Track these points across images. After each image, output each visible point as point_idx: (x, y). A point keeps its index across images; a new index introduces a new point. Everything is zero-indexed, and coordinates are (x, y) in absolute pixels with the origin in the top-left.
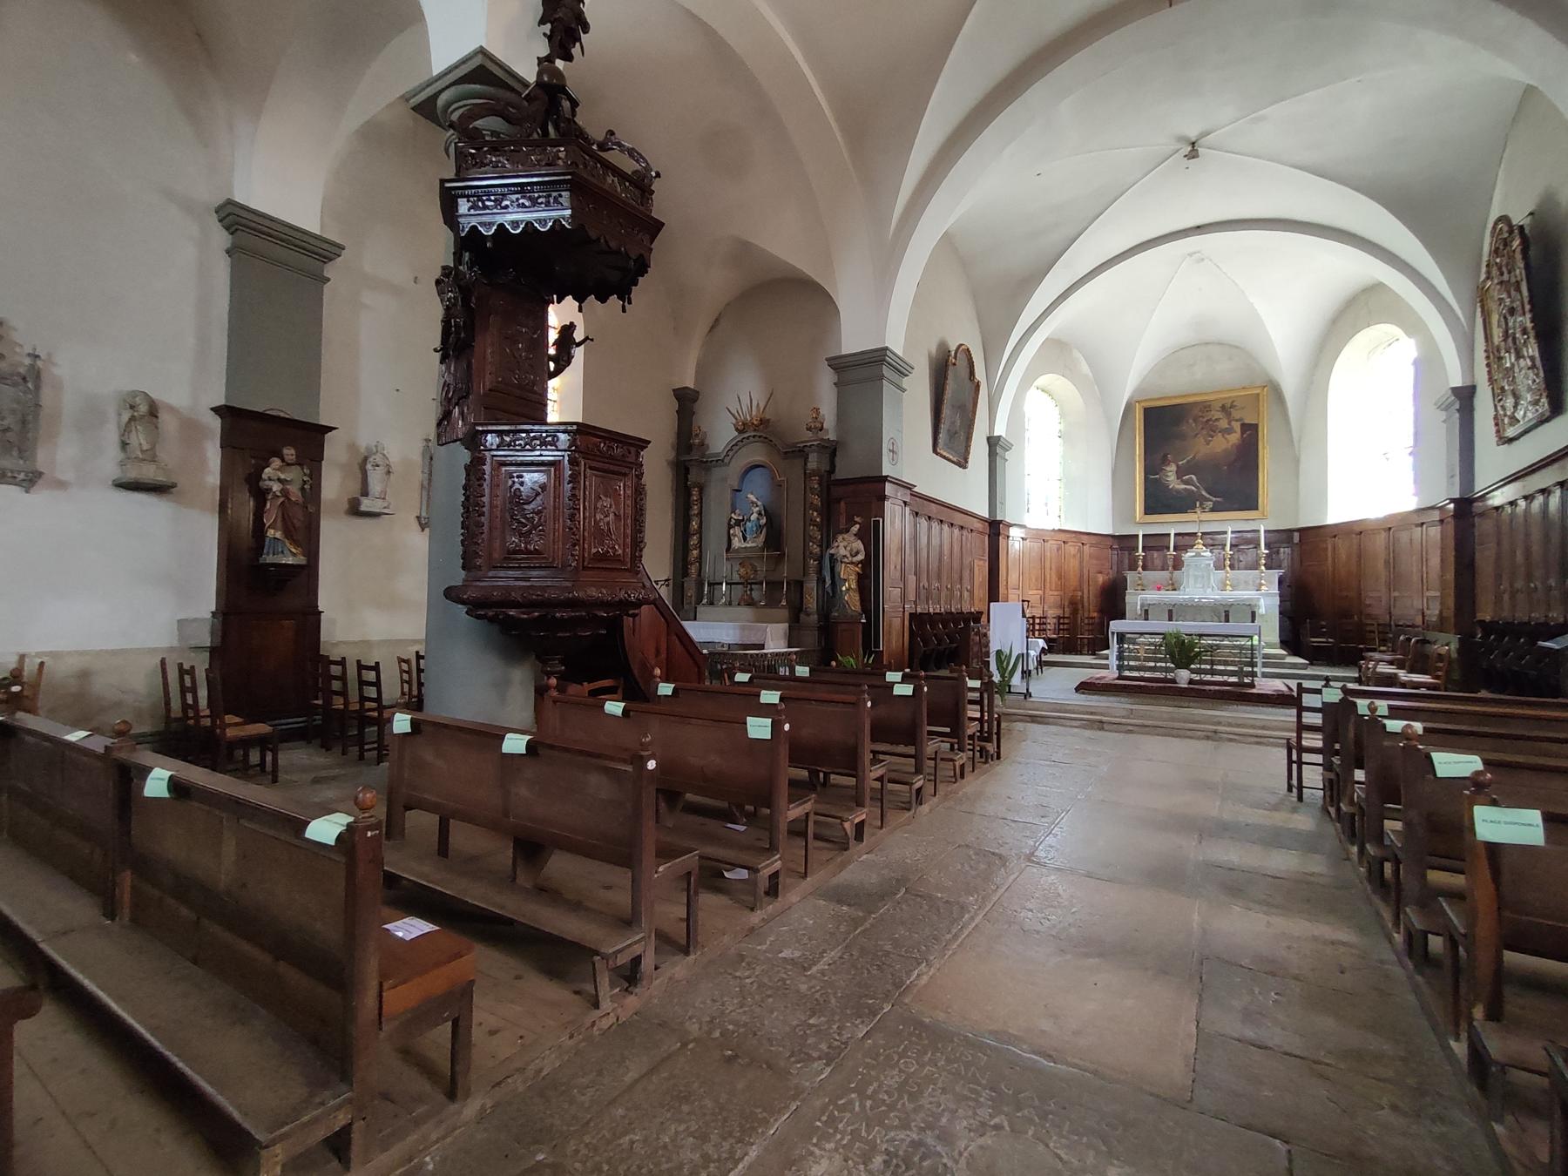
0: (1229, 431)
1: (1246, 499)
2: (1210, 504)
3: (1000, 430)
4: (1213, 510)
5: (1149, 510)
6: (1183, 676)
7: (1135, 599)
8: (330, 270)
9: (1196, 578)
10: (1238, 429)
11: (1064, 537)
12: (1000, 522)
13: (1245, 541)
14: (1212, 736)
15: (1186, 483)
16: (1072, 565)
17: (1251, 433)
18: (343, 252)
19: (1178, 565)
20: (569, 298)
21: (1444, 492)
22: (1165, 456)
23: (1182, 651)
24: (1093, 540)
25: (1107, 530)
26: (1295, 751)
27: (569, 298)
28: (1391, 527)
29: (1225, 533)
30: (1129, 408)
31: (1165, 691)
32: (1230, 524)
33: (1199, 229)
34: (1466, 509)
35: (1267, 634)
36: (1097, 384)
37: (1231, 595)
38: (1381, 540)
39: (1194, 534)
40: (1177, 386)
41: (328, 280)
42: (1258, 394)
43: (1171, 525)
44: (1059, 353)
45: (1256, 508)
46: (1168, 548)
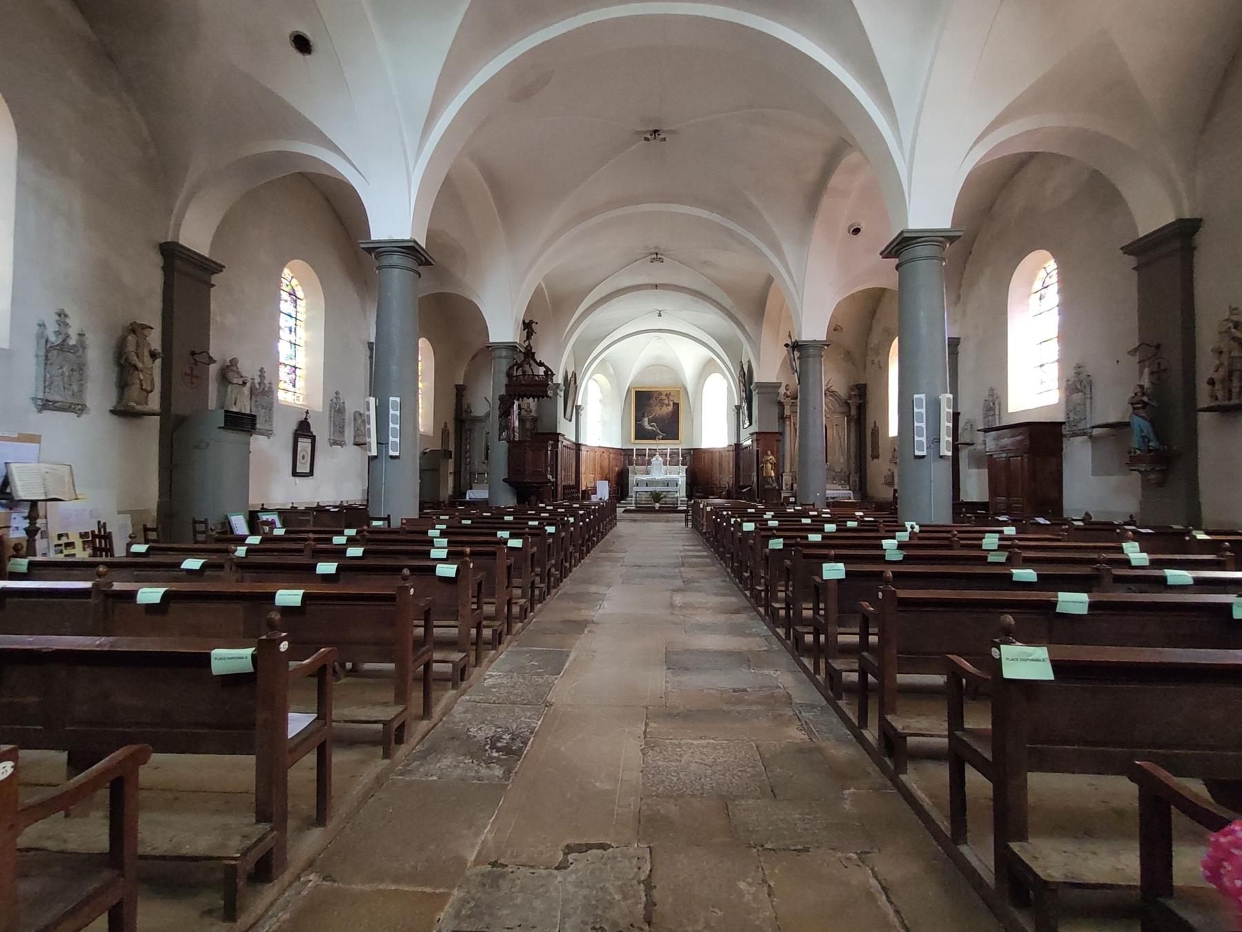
0: (668, 405)
1: (675, 436)
2: (661, 437)
3: (579, 403)
4: (662, 439)
5: (637, 438)
6: (657, 505)
7: (633, 478)
8: (215, 279)
9: (656, 469)
10: (672, 404)
11: (603, 450)
12: (559, 434)
13: (674, 453)
14: (668, 521)
15: (651, 426)
16: (606, 463)
17: (676, 405)
18: (224, 269)
19: (649, 463)
20: (531, 398)
21: (734, 441)
22: (644, 414)
23: (656, 497)
24: (614, 451)
25: (619, 446)
26: (687, 520)
27: (531, 398)
28: (720, 451)
29: (667, 449)
30: (629, 390)
31: (652, 510)
32: (668, 445)
33: (660, 330)
34: (738, 446)
35: (682, 493)
36: (616, 378)
37: (669, 476)
38: (717, 455)
39: (655, 450)
40: (648, 384)
41: (213, 285)
42: (679, 391)
43: (646, 445)
44: (602, 369)
45: (678, 439)
46: (645, 455)
